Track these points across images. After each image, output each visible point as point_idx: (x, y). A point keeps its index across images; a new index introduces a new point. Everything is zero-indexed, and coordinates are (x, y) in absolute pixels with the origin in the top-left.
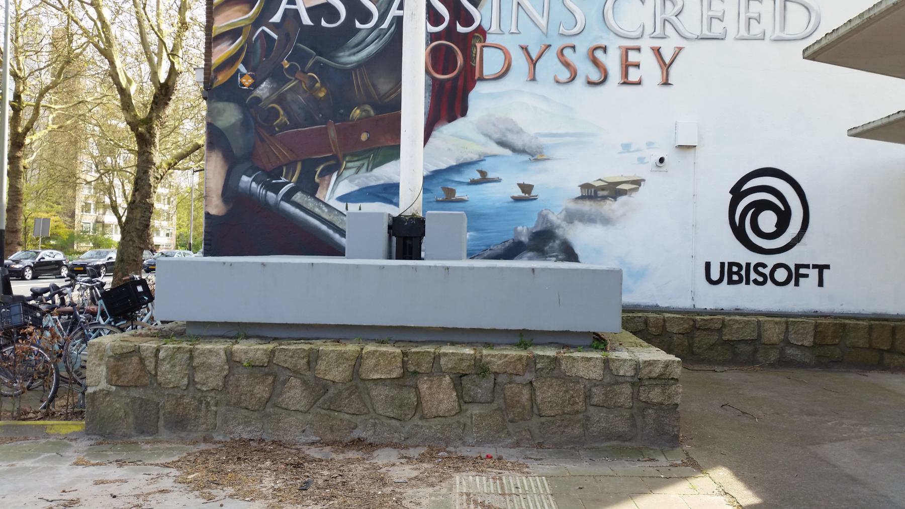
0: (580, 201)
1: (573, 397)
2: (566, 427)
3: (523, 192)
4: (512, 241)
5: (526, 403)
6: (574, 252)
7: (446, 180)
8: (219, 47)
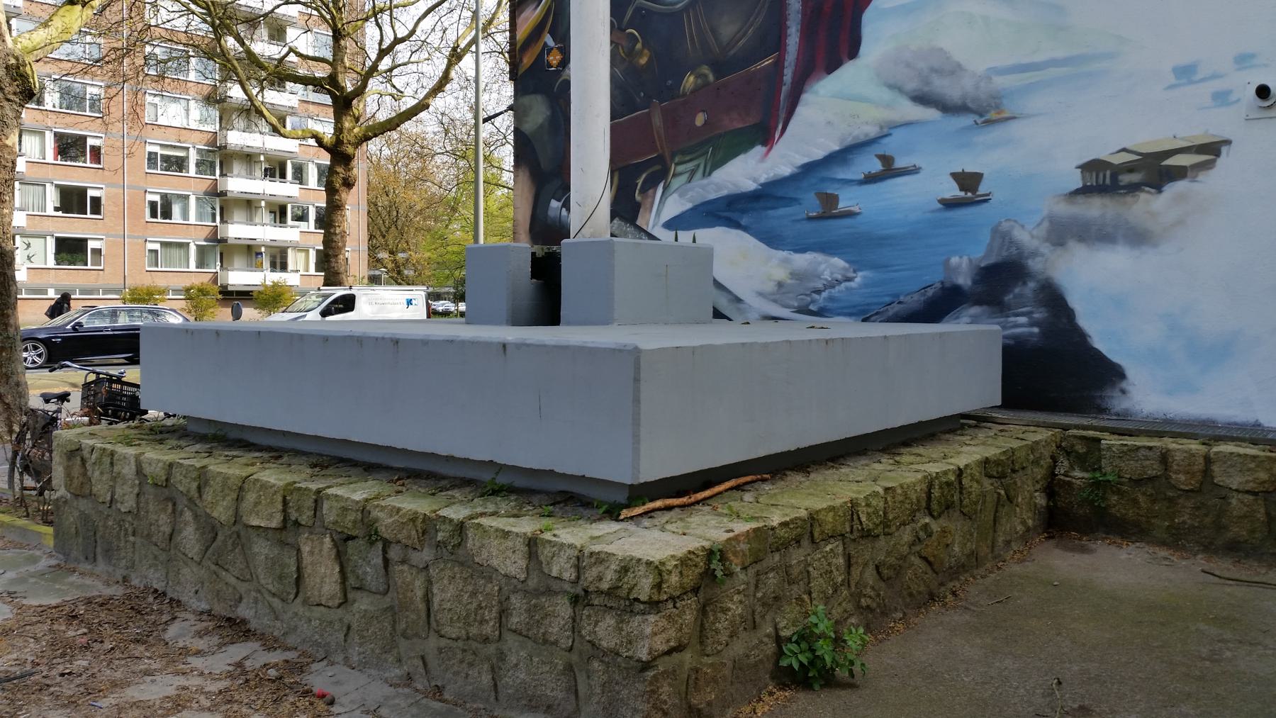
0: (1080, 199)
1: (481, 608)
2: (471, 665)
3: (961, 190)
4: (939, 285)
5: (420, 606)
6: (1067, 305)
7: (823, 180)
8: (524, 15)
